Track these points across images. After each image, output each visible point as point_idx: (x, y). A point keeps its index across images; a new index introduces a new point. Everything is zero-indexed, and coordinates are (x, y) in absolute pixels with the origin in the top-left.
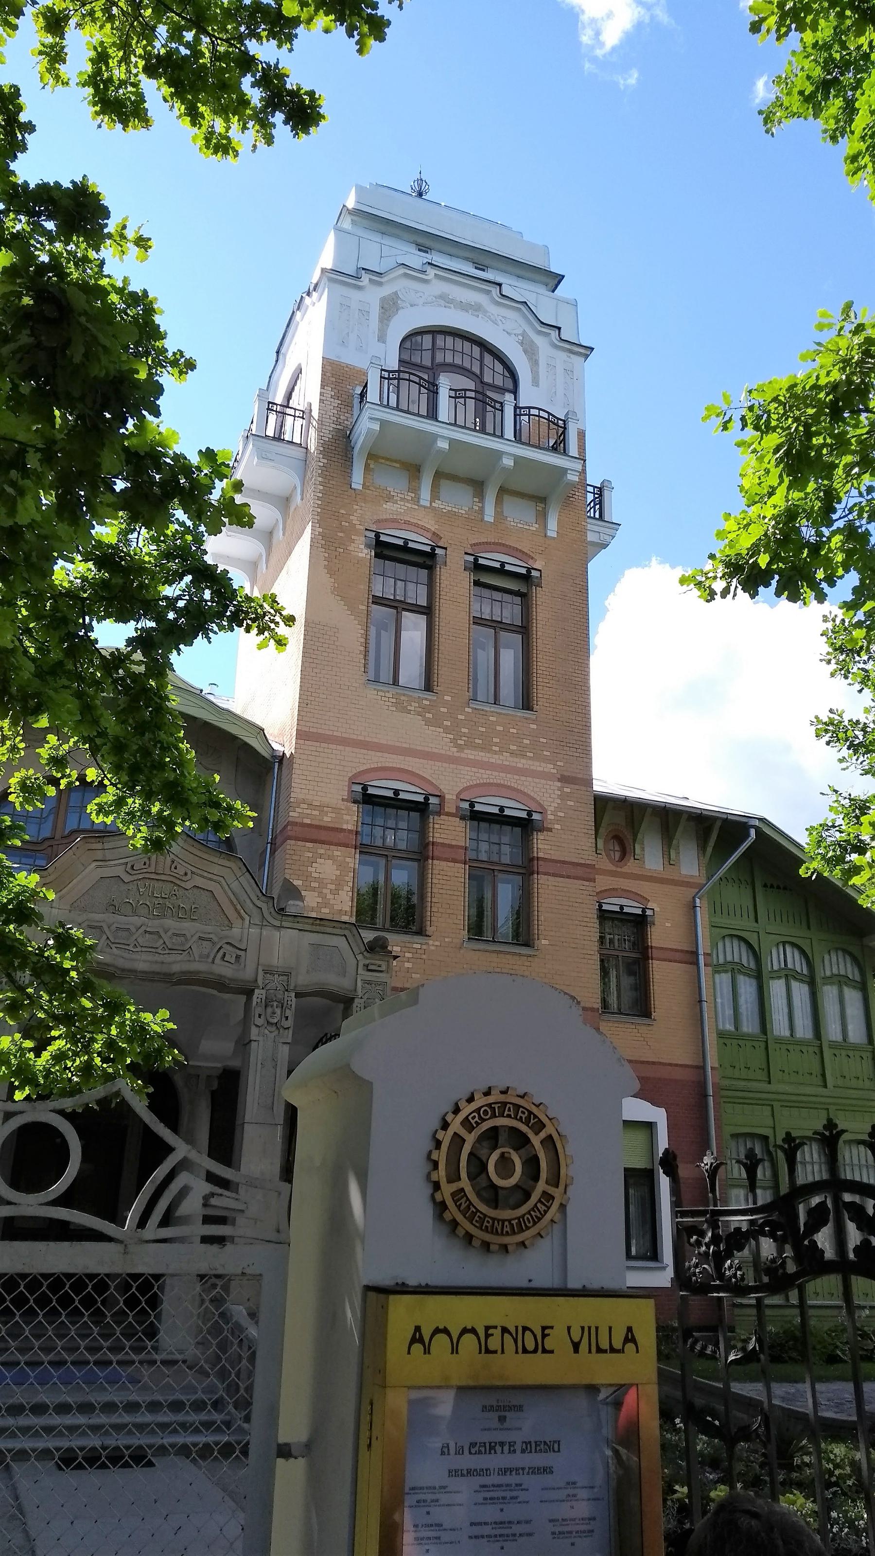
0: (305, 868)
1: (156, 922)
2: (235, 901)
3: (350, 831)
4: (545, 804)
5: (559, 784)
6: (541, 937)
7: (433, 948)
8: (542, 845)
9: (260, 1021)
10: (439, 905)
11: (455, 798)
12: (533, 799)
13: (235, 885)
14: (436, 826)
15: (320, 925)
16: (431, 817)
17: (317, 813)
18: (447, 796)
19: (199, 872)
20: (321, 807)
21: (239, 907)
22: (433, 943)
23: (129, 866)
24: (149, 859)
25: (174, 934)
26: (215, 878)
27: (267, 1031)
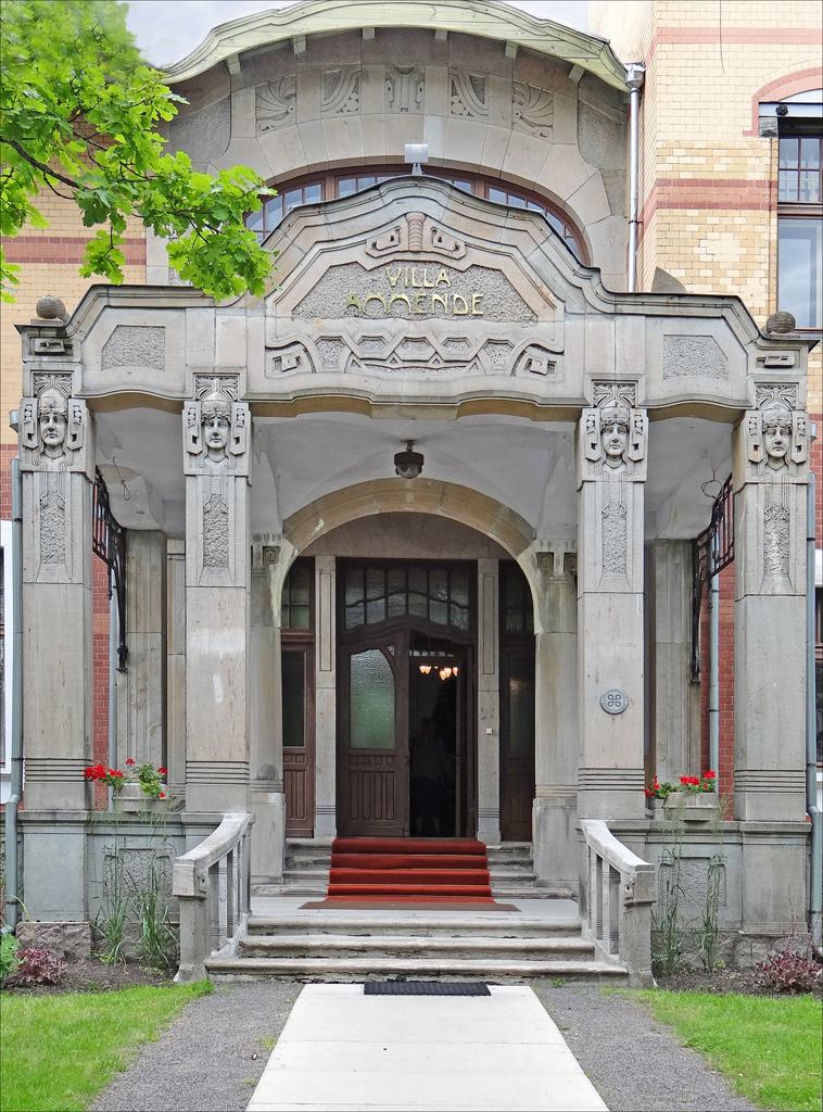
0: (689, 250)
2: (539, 283)
3: (759, 183)
15: (680, 305)
17: (702, 160)
19: (478, 243)
20: (709, 151)
21: (545, 290)
23: (369, 244)
24: (398, 230)
26: (504, 249)
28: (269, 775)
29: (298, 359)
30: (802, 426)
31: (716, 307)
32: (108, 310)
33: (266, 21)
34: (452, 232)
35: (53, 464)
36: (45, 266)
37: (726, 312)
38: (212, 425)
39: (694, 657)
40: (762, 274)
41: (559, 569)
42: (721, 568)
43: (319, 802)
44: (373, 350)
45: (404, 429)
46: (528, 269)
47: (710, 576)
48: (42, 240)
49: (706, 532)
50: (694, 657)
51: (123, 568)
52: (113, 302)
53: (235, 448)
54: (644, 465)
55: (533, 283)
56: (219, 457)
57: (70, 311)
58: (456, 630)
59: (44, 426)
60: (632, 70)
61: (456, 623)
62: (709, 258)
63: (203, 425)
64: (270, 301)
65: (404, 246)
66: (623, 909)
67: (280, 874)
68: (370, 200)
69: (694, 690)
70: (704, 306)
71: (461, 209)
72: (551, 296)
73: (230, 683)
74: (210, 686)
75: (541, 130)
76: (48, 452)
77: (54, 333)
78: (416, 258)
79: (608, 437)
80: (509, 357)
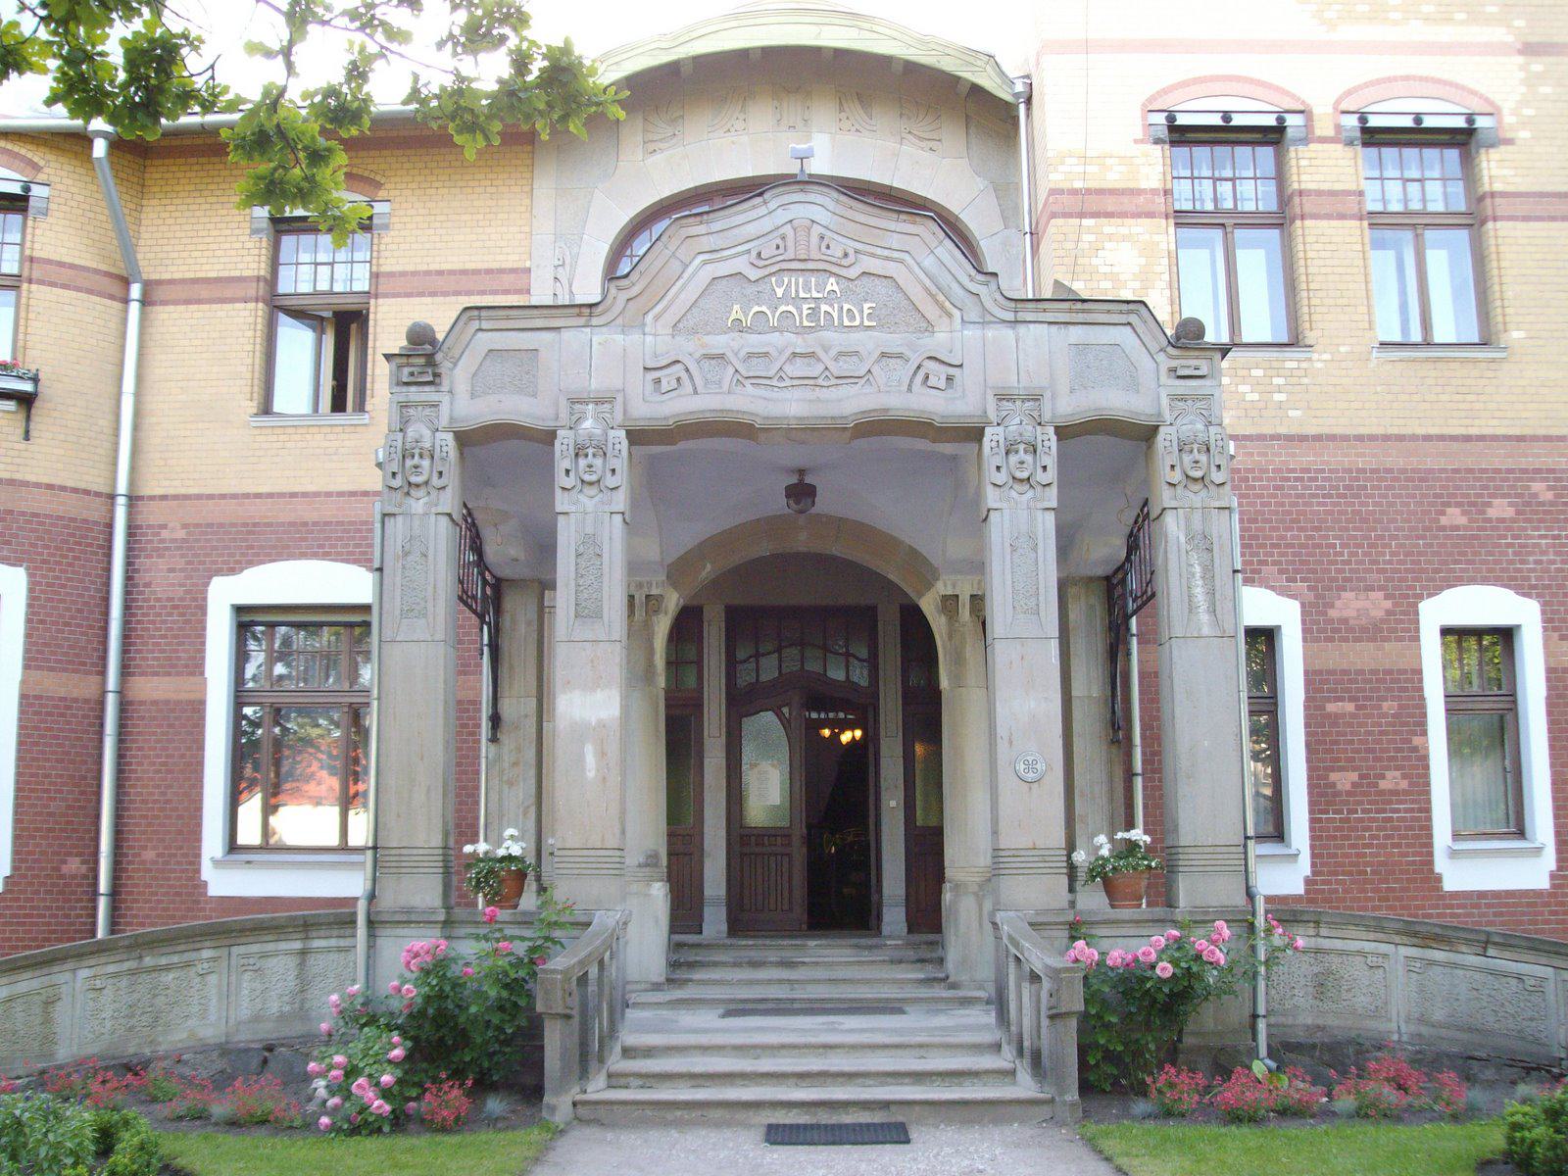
1: (810, 338)
3: (1154, 192)
4: (1497, 99)
5: (1521, 59)
6: (1509, 326)
7: (1319, 365)
8: (1496, 169)
9: (1001, 478)
10: (1320, 294)
11: (1331, 111)
12: (1474, 93)
13: (929, 262)
14: (1303, 163)
15: (1083, 311)
16: (1292, 149)
18: (1316, 111)
21: (941, 298)
22: (1319, 359)
23: (754, 254)
24: (783, 238)
25: (841, 354)
26: (896, 255)
27: (1014, 494)
28: (651, 861)
29: (678, 380)
30: (1220, 443)
31: (1121, 312)
32: (480, 334)
33: (653, 46)
34: (840, 239)
35: (418, 504)
36: (429, 300)
37: (1133, 319)
38: (586, 456)
39: (1114, 712)
40: (1164, 285)
41: (965, 613)
42: (1139, 608)
43: (708, 892)
44: (757, 368)
45: (795, 457)
46: (922, 276)
47: (1127, 618)
48: (428, 273)
49: (1120, 568)
50: (1114, 712)
51: (497, 624)
52: (485, 325)
53: (610, 481)
54: (1054, 490)
55: (927, 290)
56: (593, 491)
57: (440, 337)
58: (855, 687)
59: (409, 463)
60: (1019, 87)
61: (855, 679)
62: (1107, 269)
63: (577, 455)
64: (650, 317)
65: (790, 254)
66: (1045, 1022)
67: (662, 979)
68: (754, 207)
69: (1114, 750)
70: (1109, 312)
71: (849, 214)
72: (947, 304)
73: (603, 754)
74: (581, 759)
75: (931, 144)
76: (412, 492)
77: (422, 361)
78: (803, 266)
79: (1013, 459)
80: (903, 372)
